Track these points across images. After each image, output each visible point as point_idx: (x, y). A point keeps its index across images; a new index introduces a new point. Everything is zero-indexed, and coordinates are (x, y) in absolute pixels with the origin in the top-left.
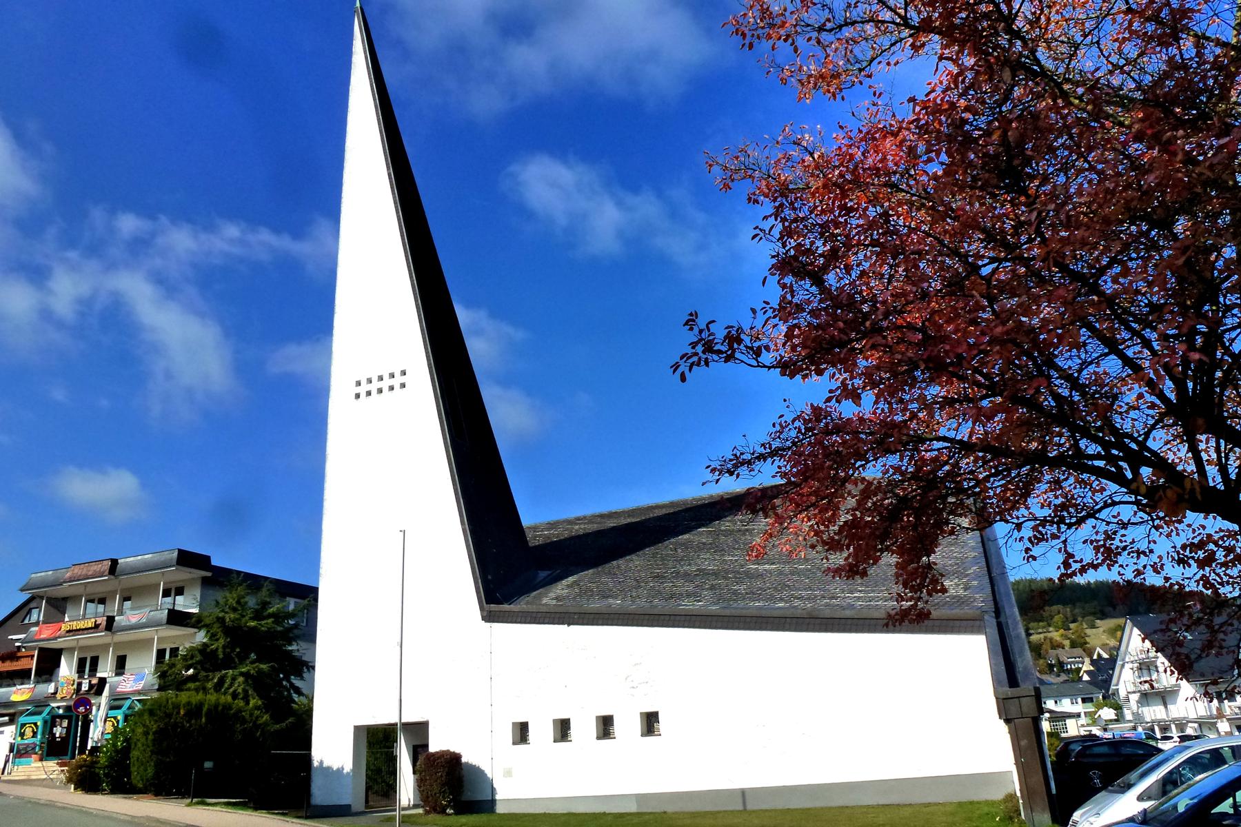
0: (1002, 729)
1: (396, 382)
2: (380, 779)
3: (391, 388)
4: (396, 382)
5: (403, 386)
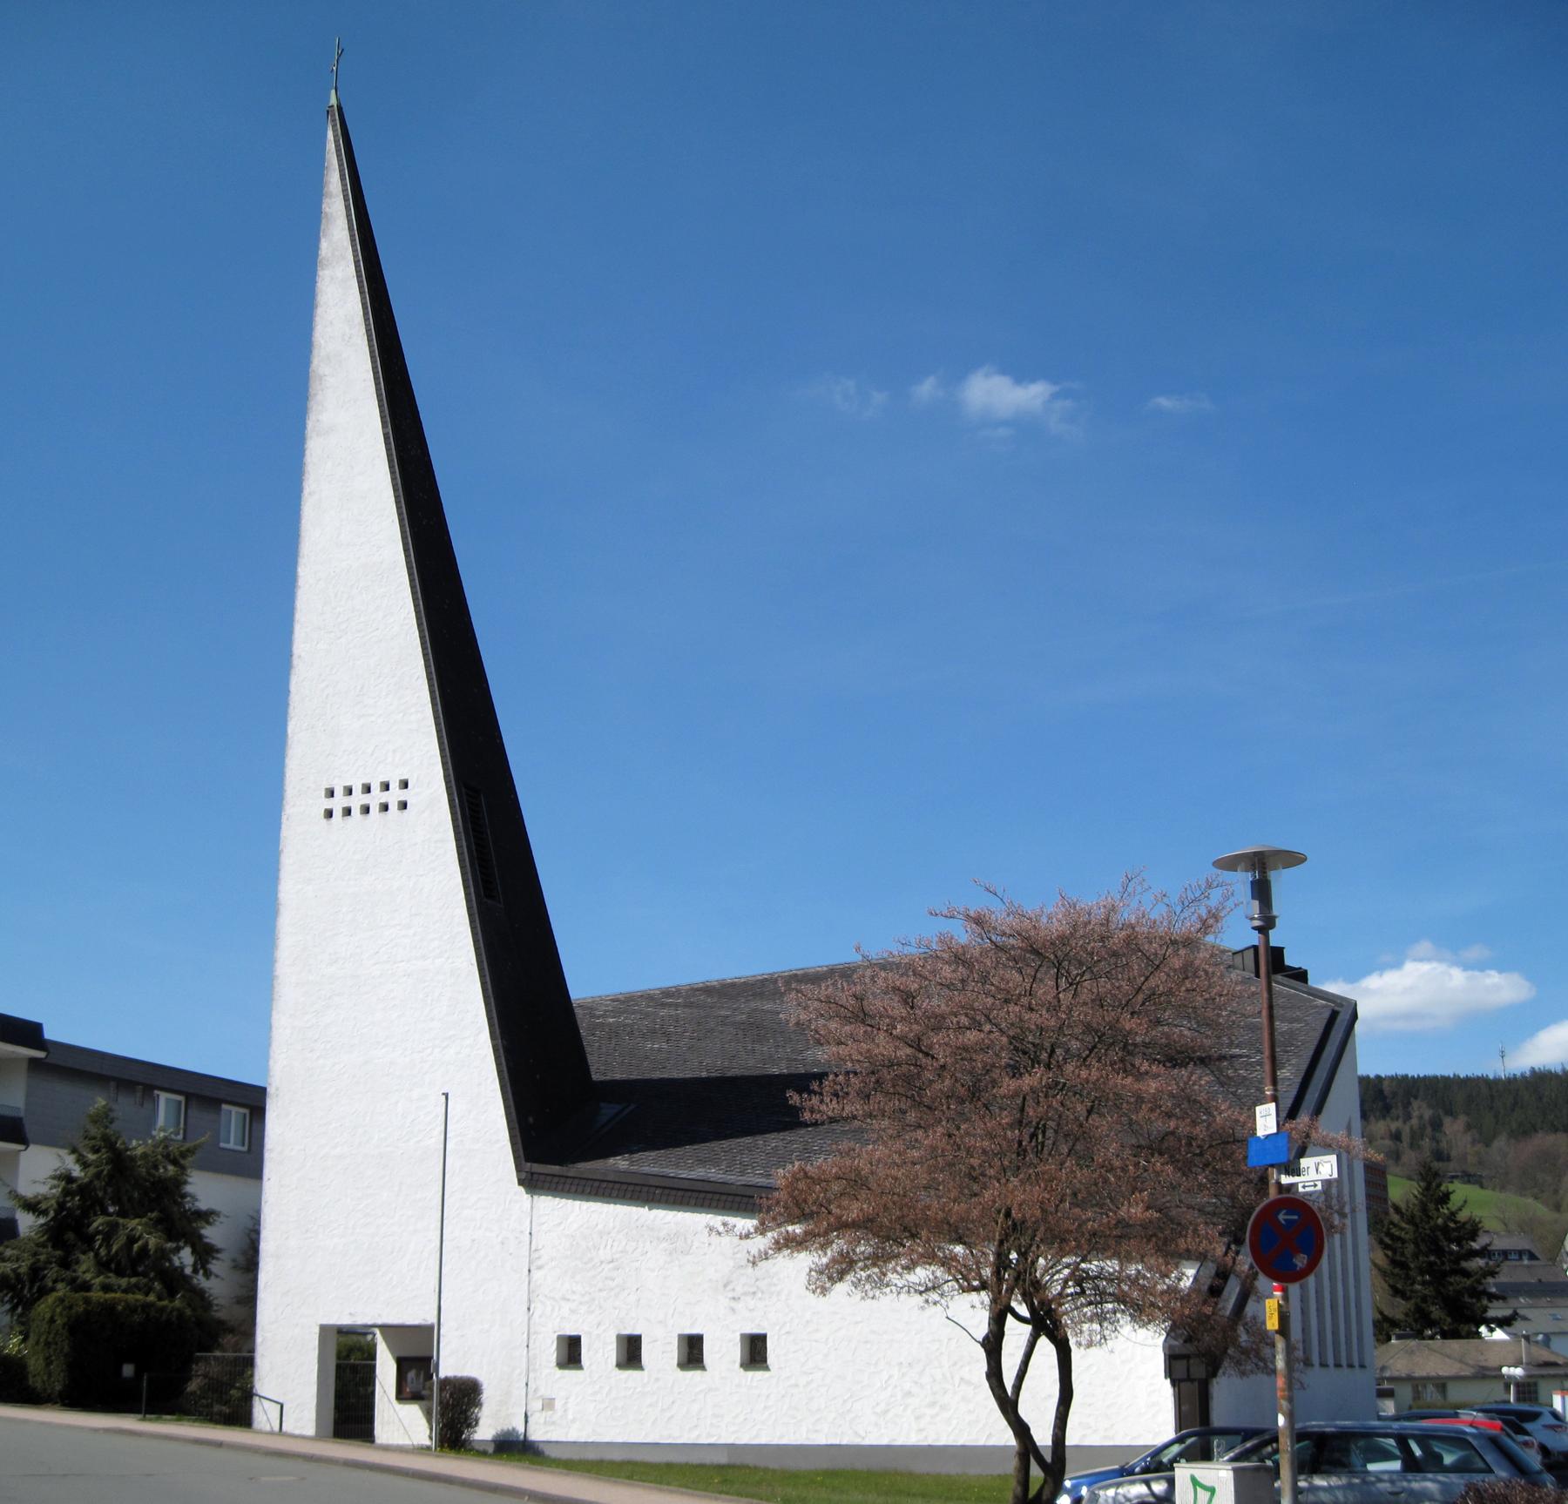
0: (1166, 1390)
1: (338, 803)
2: (350, 1412)
3: (385, 807)
4: (338, 803)
5: (403, 805)
